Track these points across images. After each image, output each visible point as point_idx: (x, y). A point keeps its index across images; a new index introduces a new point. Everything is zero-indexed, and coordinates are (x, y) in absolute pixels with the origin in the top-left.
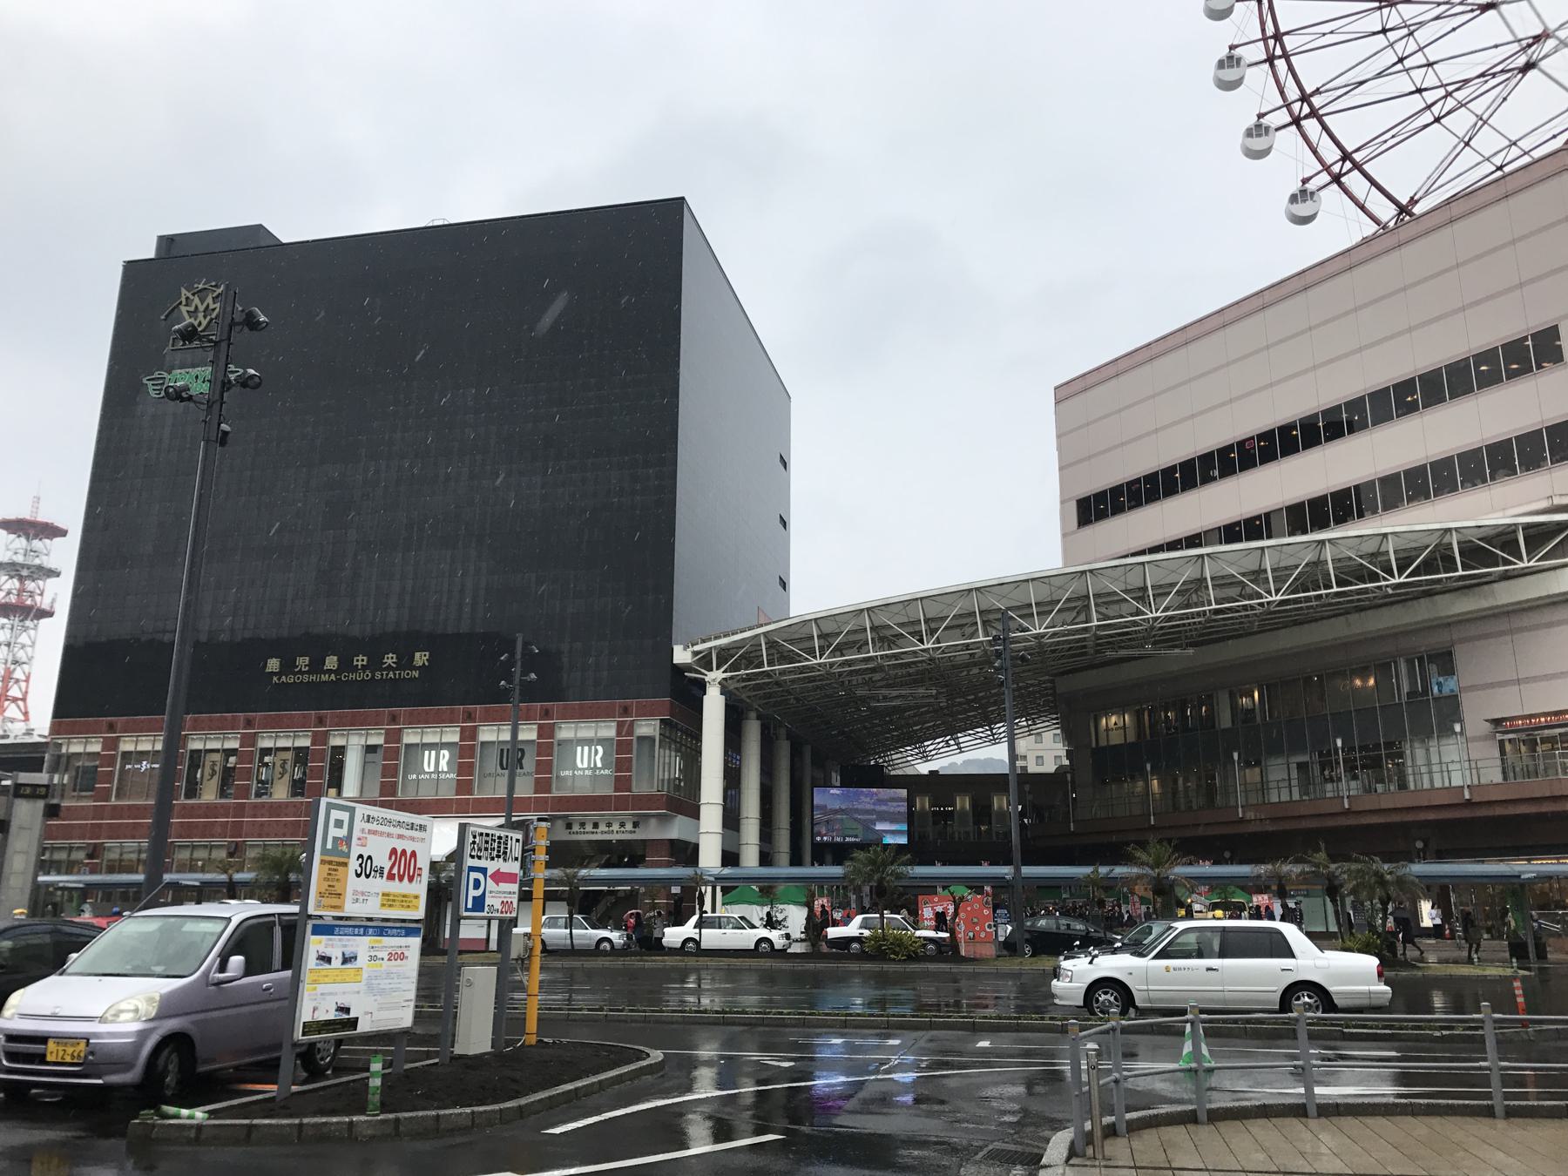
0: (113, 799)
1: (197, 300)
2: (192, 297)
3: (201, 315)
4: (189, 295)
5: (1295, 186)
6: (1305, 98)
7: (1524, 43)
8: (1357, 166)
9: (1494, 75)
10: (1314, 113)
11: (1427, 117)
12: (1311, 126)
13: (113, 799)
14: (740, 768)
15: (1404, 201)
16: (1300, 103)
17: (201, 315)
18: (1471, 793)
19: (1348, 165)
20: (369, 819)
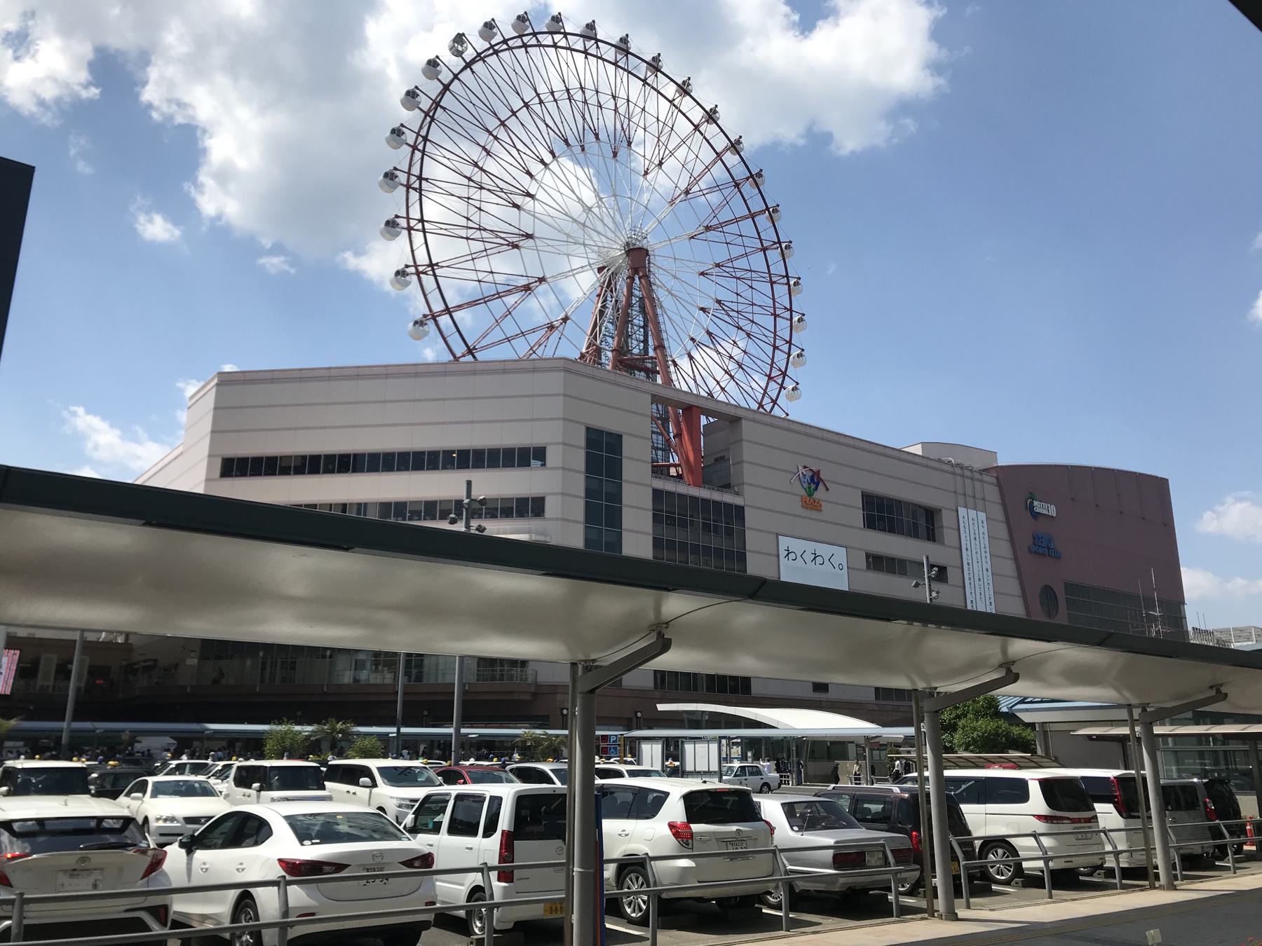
0: (1114, 881)
5: (401, 267)
6: (420, 178)
7: (522, 233)
8: (424, 231)
9: (497, 237)
10: (420, 190)
11: (463, 233)
12: (418, 155)
13: (1114, 881)
14: (889, 914)
15: (434, 262)
16: (416, 178)
18: (469, 687)
19: (421, 269)
20: (531, 507)
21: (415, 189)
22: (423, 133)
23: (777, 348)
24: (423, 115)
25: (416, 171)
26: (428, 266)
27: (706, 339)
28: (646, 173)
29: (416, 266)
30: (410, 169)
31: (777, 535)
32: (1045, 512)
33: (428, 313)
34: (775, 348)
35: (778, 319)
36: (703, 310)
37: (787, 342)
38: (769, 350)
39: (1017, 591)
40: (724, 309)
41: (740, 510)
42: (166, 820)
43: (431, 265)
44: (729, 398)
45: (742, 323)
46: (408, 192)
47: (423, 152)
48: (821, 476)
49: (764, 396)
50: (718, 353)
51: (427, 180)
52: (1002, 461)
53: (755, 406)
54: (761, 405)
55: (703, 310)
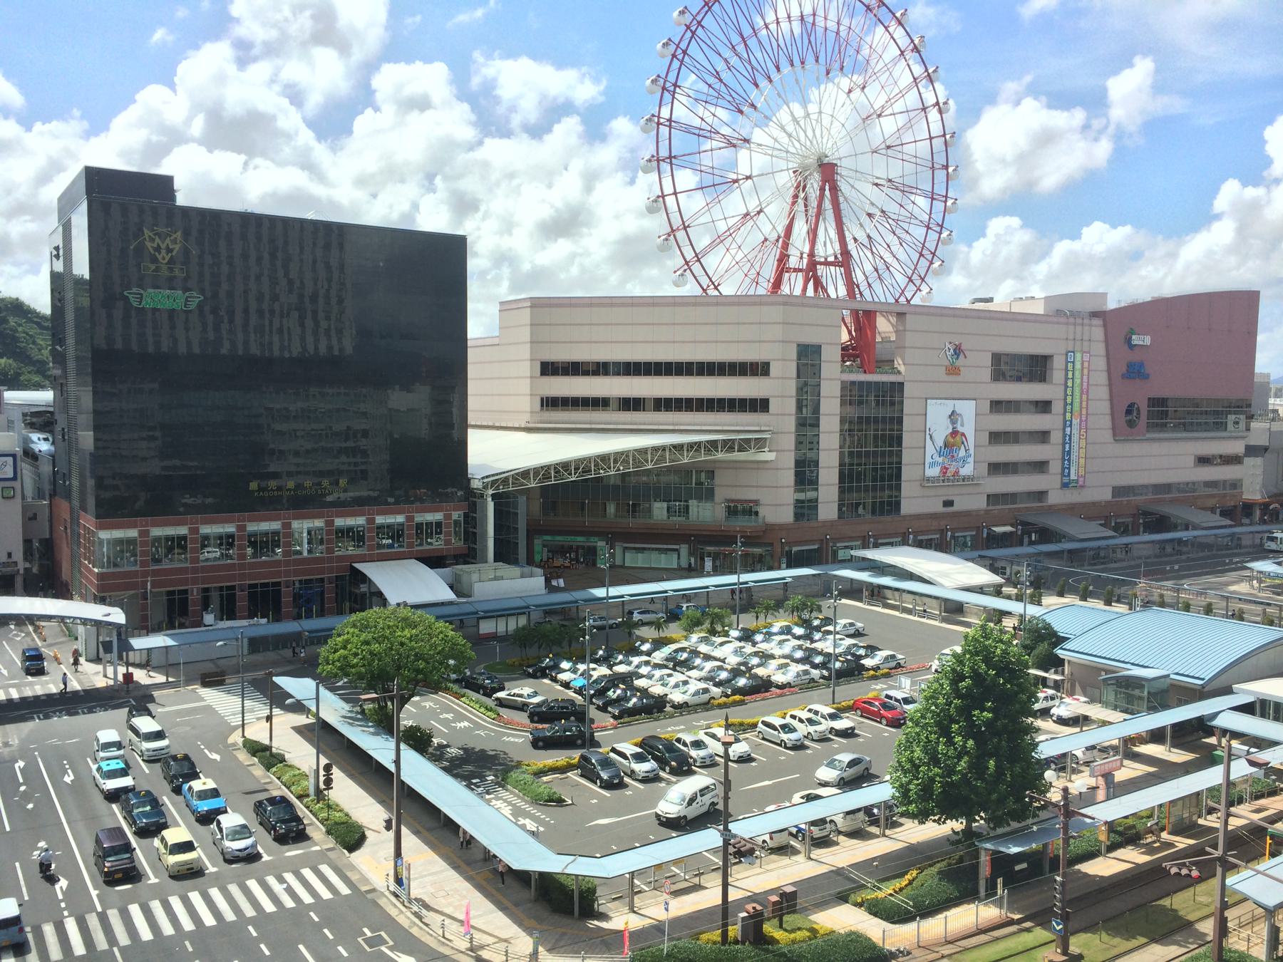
1: (157, 240)
2: (178, 242)
3: (163, 252)
4: (151, 234)
17: (163, 252)
21: (691, 31)
22: (699, 18)
23: (923, 255)
24: (703, 3)
25: (683, 45)
26: (668, 120)
27: (866, 242)
28: (850, 91)
29: (659, 117)
30: (679, 43)
31: (926, 399)
32: (1141, 343)
33: (655, 154)
34: (910, 280)
35: (922, 258)
36: (870, 215)
37: (932, 253)
38: (915, 256)
39: (1108, 411)
40: (871, 250)
41: (901, 384)
42: (154, 751)
43: (670, 120)
44: (875, 296)
45: (898, 231)
46: (686, 31)
47: (682, 62)
48: (962, 348)
49: (901, 294)
50: (872, 253)
51: (703, 27)
52: (1112, 305)
53: (892, 301)
54: (897, 301)
55: (870, 215)
